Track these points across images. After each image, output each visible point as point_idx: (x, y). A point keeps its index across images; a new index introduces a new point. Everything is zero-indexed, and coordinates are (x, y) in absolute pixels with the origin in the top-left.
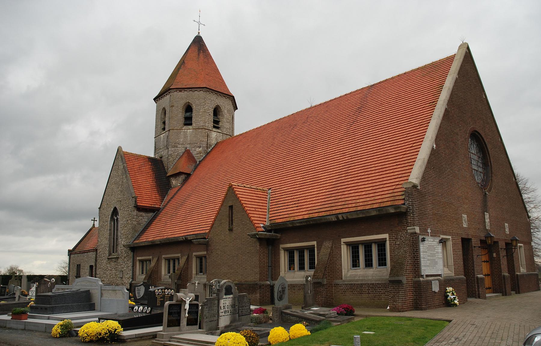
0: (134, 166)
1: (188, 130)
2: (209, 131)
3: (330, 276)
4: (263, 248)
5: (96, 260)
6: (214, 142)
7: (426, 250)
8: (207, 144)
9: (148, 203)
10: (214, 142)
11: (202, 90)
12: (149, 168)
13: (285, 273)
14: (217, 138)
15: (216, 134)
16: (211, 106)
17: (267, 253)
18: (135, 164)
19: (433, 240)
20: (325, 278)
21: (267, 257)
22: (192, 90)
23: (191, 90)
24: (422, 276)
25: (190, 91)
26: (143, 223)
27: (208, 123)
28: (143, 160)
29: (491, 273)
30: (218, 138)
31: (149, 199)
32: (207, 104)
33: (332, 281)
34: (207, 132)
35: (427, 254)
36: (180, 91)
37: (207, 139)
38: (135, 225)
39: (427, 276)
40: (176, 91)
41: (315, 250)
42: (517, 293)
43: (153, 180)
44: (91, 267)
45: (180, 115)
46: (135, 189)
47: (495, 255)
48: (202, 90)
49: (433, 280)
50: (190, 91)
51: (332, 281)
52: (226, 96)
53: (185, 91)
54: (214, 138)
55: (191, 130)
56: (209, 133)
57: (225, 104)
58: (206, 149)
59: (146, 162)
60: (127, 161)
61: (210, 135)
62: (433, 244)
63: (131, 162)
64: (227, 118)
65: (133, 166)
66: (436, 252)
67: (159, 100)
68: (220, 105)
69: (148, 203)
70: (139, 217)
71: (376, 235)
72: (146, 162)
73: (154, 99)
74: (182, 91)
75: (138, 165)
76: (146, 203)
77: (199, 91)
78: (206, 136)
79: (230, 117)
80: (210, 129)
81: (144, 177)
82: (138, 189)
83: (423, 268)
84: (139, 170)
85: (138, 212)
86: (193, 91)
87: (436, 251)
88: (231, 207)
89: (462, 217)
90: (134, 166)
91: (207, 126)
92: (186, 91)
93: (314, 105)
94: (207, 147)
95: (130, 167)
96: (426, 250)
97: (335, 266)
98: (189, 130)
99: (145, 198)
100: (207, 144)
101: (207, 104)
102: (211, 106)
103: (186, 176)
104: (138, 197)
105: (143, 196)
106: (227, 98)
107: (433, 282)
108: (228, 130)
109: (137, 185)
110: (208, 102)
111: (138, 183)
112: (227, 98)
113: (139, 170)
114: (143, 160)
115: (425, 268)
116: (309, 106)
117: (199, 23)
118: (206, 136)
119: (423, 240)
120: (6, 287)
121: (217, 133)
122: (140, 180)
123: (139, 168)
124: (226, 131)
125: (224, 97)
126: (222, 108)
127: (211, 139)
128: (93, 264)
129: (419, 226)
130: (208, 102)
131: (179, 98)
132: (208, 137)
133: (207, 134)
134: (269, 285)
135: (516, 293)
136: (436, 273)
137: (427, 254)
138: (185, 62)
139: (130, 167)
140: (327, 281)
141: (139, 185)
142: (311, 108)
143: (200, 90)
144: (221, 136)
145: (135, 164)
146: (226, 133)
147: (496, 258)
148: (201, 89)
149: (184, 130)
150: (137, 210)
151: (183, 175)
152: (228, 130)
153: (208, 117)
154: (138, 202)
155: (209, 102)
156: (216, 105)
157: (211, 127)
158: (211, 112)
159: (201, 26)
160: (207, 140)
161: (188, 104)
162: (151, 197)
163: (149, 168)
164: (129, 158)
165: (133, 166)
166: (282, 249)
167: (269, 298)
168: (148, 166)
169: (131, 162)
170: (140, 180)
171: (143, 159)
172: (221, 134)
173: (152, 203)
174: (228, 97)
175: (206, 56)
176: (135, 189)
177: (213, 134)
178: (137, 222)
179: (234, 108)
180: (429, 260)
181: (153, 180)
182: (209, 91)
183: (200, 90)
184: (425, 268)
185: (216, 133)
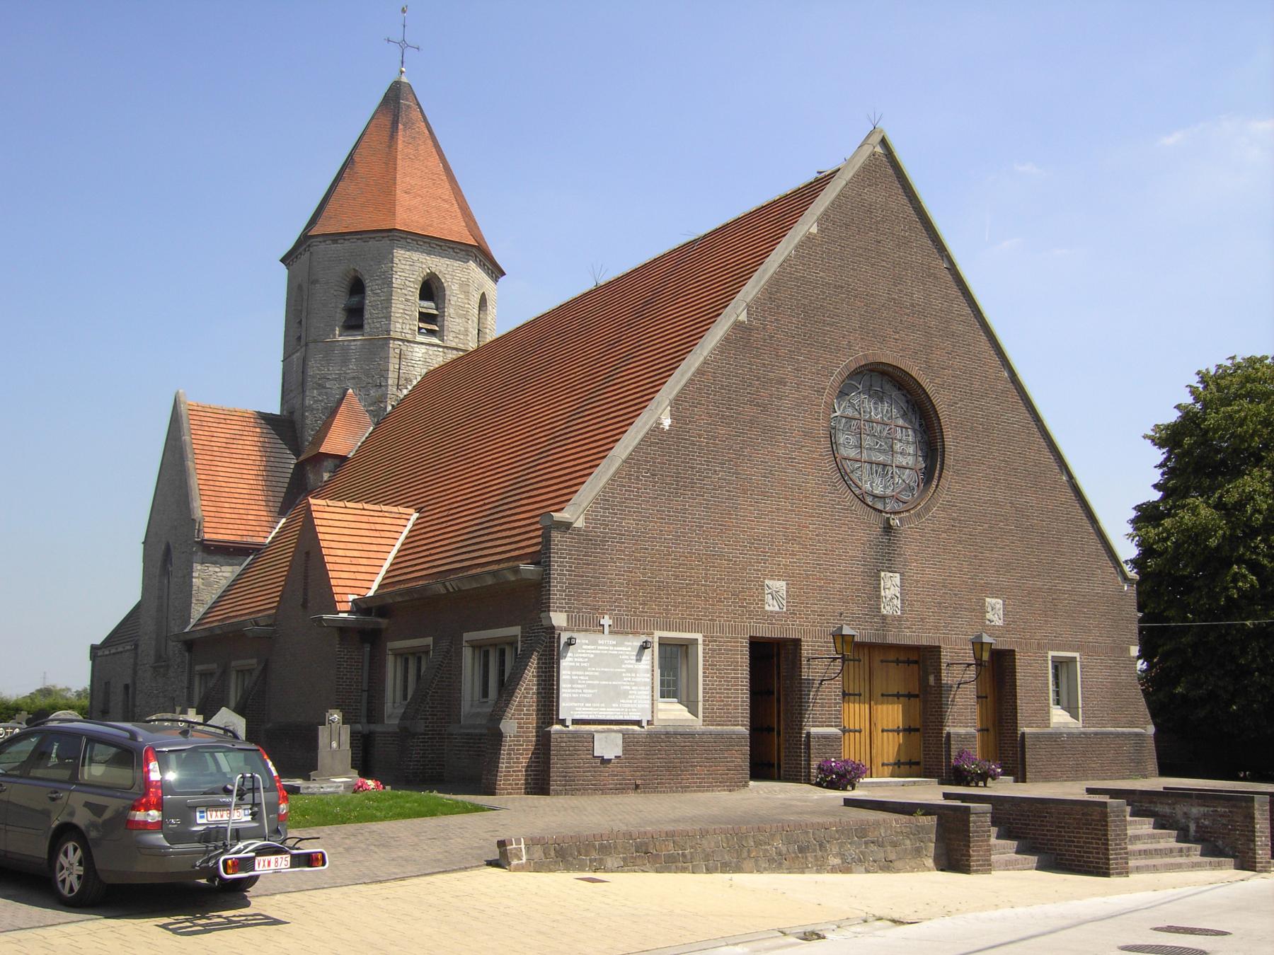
0: (213, 439)
1: (352, 343)
2: (406, 343)
3: (436, 715)
4: (350, 650)
5: (135, 672)
6: (419, 370)
7: (585, 664)
8: (399, 376)
9: (234, 532)
10: (419, 370)
11: (388, 236)
12: (253, 443)
13: (394, 706)
14: (428, 360)
15: (424, 351)
16: (411, 276)
17: (361, 660)
18: (215, 434)
19: (615, 643)
20: (421, 719)
21: (359, 669)
22: (363, 236)
23: (359, 237)
24: (563, 722)
25: (358, 239)
26: (221, 581)
27: (401, 321)
28: (240, 423)
29: (923, 726)
30: (430, 361)
31: (238, 522)
32: (399, 273)
33: (444, 727)
34: (398, 346)
35: (587, 673)
36: (335, 242)
37: (400, 364)
38: (198, 587)
39: (575, 722)
40: (325, 241)
41: (1068, 656)
42: (1019, 780)
43: (259, 473)
44: (127, 687)
45: (338, 303)
46: (205, 498)
47: (932, 679)
48: (388, 236)
49: (597, 732)
50: (358, 239)
51: (444, 727)
52: (455, 246)
53: (346, 242)
54: (420, 361)
55: (359, 343)
56: (404, 348)
57: (455, 268)
58: (395, 390)
59: (247, 429)
60: (195, 427)
61: (406, 353)
62: (616, 652)
63: (206, 428)
64: (461, 304)
65: (209, 438)
66: (624, 670)
67: (295, 260)
68: (437, 273)
69: (234, 532)
70: (210, 569)
71: (507, 627)
72: (247, 429)
73: (283, 260)
74: (337, 240)
75: (223, 435)
76: (229, 532)
77: (381, 238)
78: (395, 357)
79: (466, 301)
80: (409, 337)
81: (237, 466)
82: (213, 499)
83: (563, 704)
84: (223, 450)
85: (205, 555)
86: (351, 240)
87: (623, 666)
88: (307, 554)
89: (763, 586)
90: (213, 439)
91: (401, 330)
92: (349, 240)
93: (602, 282)
94: (398, 385)
95: (201, 442)
96: (585, 664)
97: (545, 701)
98: (355, 343)
99: (228, 521)
100: (398, 379)
101: (399, 273)
102: (411, 276)
103: (337, 462)
104: (207, 519)
105: (223, 515)
106: (458, 251)
107: (596, 736)
108: (462, 337)
109: (212, 488)
110: (403, 267)
111: (217, 484)
112: (458, 251)
113: (223, 450)
114: (240, 423)
115: (576, 705)
116: (591, 286)
117: (403, 45)
118: (395, 357)
119: (570, 643)
120: (1248, 798)
121: (427, 347)
122: (221, 474)
123: (224, 445)
124: (457, 340)
125: (449, 250)
126: (447, 281)
127: (409, 364)
128: (129, 681)
129: (566, 612)
130: (403, 267)
131: (332, 259)
132: (400, 359)
133: (398, 352)
134: (359, 733)
135: (1016, 781)
136: (621, 718)
137: (587, 673)
138: (356, 159)
139: (201, 442)
140: (426, 727)
141: (217, 489)
142: (598, 289)
143: (383, 237)
144: (441, 354)
145: (215, 434)
146: (453, 345)
147: (934, 687)
148: (386, 234)
149: (341, 343)
150: (203, 551)
151: (329, 459)
152: (462, 337)
153: (403, 307)
154: (206, 530)
155: (408, 267)
156: (428, 274)
157: (410, 332)
158: (411, 293)
159: (408, 52)
160: (398, 367)
161: (352, 273)
162: (245, 517)
163: (253, 443)
164: (203, 419)
165: (209, 438)
166: (390, 653)
167: (359, 760)
168: (250, 438)
169: (206, 428)
170: (221, 474)
171: (241, 419)
172: (441, 350)
173: (245, 533)
174: (461, 250)
175: (414, 138)
176: (205, 498)
177: (418, 350)
178: (202, 579)
179: (492, 272)
180: (589, 687)
181: (259, 473)
182: (406, 238)
183: (383, 237)
184: (576, 705)
185: (424, 346)
